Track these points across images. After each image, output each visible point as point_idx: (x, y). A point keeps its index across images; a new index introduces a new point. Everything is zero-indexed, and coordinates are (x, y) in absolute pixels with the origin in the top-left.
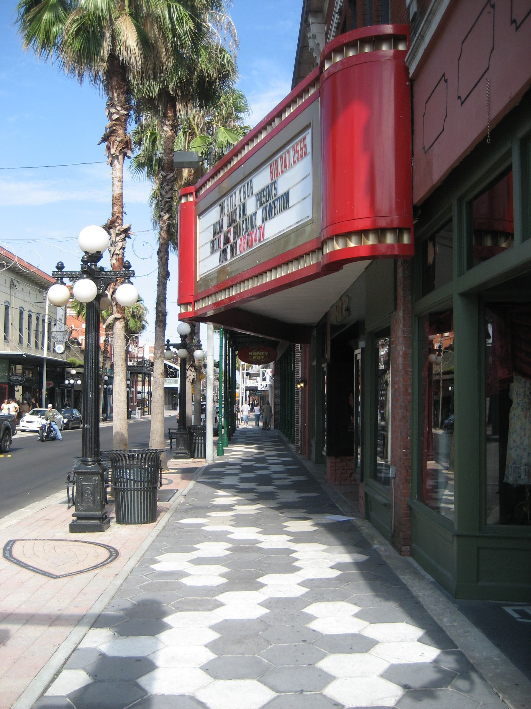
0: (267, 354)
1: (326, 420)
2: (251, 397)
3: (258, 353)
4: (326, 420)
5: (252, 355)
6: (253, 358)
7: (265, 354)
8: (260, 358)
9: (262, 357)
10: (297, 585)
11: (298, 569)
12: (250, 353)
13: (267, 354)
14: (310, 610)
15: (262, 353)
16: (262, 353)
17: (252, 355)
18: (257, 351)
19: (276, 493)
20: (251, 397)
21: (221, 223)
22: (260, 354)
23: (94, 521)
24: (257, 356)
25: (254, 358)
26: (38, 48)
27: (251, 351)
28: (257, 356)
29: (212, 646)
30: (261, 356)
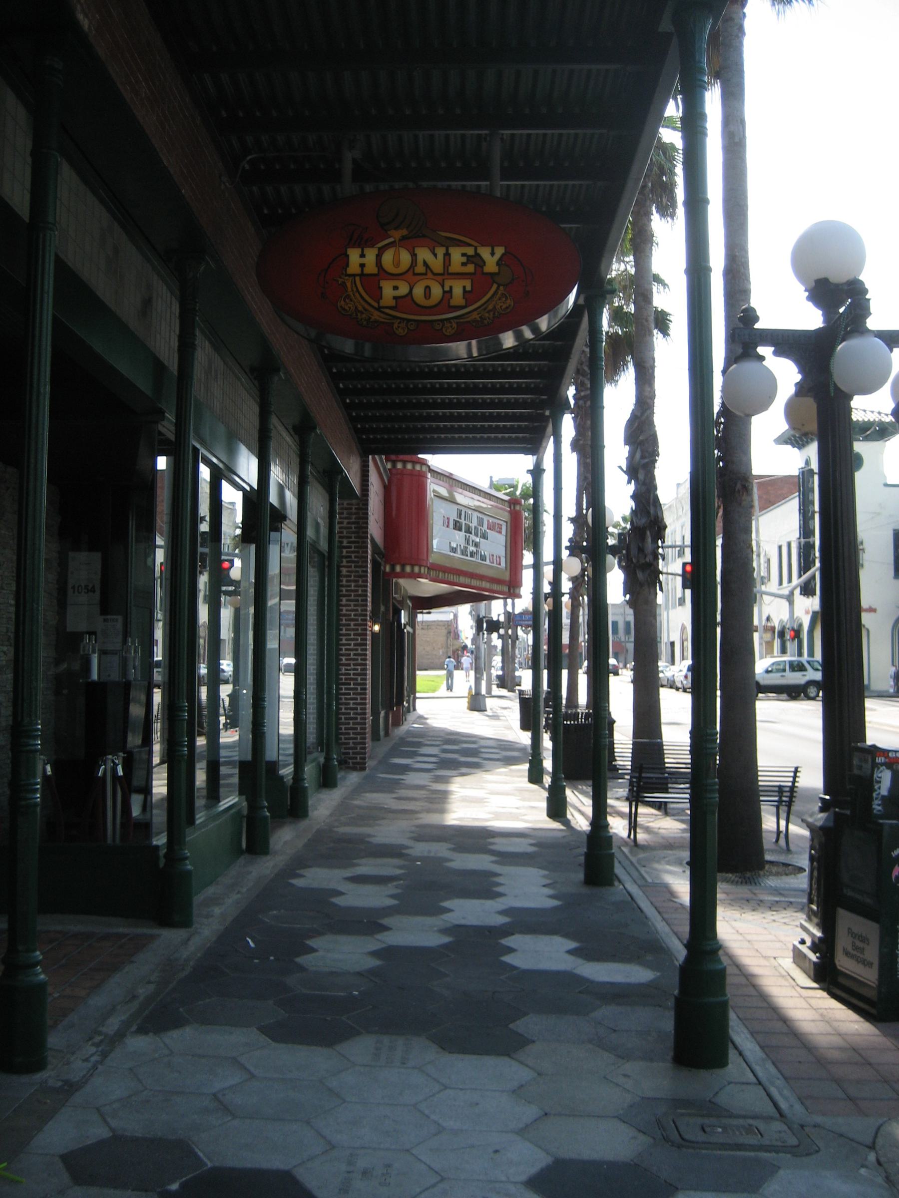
0: (491, 259)
1: (158, 676)
2: (493, 693)
3: (424, 254)
4: (158, 676)
5: (371, 268)
6: (377, 294)
7: (476, 260)
8: (437, 291)
9: (458, 288)
10: (454, 909)
11: (500, 895)
12: (354, 255)
13: (491, 259)
14: (509, 941)
15: (457, 255)
16: (457, 255)
17: (371, 268)
18: (410, 242)
19: (486, 799)
20: (493, 693)
21: (662, 1133)
22: (437, 264)
23: (188, 529)
24: (411, 274)
25: (388, 291)
26: (508, 676)
27: (362, 243)
28: (411, 274)
29: (265, 723)
30: (446, 274)
